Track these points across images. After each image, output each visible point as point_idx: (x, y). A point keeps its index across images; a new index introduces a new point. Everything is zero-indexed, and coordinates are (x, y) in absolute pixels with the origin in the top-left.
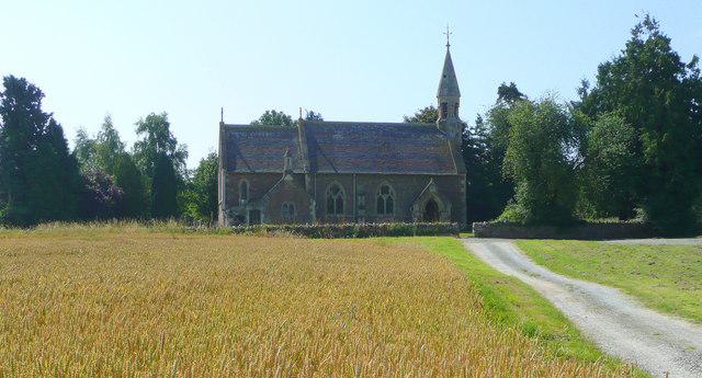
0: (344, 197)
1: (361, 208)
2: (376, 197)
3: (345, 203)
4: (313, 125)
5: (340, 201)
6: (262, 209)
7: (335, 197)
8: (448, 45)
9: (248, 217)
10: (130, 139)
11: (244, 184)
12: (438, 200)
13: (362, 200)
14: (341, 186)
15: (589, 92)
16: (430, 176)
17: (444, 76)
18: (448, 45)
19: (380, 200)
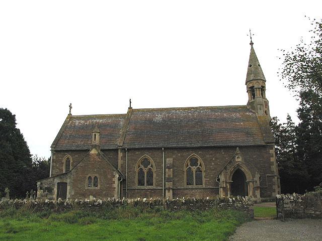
0: (154, 170)
1: (168, 180)
2: (185, 169)
3: (155, 175)
4: (21, 136)
5: (150, 174)
6: (68, 181)
7: (145, 171)
8: (252, 44)
9: (55, 190)
10: (13, 114)
11: (68, 161)
12: (244, 169)
13: (170, 172)
14: (151, 161)
15: (279, 176)
16: (237, 146)
17: (250, 66)
18: (252, 44)
19: (189, 172)
